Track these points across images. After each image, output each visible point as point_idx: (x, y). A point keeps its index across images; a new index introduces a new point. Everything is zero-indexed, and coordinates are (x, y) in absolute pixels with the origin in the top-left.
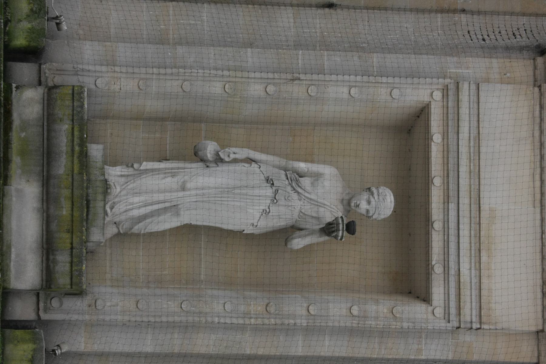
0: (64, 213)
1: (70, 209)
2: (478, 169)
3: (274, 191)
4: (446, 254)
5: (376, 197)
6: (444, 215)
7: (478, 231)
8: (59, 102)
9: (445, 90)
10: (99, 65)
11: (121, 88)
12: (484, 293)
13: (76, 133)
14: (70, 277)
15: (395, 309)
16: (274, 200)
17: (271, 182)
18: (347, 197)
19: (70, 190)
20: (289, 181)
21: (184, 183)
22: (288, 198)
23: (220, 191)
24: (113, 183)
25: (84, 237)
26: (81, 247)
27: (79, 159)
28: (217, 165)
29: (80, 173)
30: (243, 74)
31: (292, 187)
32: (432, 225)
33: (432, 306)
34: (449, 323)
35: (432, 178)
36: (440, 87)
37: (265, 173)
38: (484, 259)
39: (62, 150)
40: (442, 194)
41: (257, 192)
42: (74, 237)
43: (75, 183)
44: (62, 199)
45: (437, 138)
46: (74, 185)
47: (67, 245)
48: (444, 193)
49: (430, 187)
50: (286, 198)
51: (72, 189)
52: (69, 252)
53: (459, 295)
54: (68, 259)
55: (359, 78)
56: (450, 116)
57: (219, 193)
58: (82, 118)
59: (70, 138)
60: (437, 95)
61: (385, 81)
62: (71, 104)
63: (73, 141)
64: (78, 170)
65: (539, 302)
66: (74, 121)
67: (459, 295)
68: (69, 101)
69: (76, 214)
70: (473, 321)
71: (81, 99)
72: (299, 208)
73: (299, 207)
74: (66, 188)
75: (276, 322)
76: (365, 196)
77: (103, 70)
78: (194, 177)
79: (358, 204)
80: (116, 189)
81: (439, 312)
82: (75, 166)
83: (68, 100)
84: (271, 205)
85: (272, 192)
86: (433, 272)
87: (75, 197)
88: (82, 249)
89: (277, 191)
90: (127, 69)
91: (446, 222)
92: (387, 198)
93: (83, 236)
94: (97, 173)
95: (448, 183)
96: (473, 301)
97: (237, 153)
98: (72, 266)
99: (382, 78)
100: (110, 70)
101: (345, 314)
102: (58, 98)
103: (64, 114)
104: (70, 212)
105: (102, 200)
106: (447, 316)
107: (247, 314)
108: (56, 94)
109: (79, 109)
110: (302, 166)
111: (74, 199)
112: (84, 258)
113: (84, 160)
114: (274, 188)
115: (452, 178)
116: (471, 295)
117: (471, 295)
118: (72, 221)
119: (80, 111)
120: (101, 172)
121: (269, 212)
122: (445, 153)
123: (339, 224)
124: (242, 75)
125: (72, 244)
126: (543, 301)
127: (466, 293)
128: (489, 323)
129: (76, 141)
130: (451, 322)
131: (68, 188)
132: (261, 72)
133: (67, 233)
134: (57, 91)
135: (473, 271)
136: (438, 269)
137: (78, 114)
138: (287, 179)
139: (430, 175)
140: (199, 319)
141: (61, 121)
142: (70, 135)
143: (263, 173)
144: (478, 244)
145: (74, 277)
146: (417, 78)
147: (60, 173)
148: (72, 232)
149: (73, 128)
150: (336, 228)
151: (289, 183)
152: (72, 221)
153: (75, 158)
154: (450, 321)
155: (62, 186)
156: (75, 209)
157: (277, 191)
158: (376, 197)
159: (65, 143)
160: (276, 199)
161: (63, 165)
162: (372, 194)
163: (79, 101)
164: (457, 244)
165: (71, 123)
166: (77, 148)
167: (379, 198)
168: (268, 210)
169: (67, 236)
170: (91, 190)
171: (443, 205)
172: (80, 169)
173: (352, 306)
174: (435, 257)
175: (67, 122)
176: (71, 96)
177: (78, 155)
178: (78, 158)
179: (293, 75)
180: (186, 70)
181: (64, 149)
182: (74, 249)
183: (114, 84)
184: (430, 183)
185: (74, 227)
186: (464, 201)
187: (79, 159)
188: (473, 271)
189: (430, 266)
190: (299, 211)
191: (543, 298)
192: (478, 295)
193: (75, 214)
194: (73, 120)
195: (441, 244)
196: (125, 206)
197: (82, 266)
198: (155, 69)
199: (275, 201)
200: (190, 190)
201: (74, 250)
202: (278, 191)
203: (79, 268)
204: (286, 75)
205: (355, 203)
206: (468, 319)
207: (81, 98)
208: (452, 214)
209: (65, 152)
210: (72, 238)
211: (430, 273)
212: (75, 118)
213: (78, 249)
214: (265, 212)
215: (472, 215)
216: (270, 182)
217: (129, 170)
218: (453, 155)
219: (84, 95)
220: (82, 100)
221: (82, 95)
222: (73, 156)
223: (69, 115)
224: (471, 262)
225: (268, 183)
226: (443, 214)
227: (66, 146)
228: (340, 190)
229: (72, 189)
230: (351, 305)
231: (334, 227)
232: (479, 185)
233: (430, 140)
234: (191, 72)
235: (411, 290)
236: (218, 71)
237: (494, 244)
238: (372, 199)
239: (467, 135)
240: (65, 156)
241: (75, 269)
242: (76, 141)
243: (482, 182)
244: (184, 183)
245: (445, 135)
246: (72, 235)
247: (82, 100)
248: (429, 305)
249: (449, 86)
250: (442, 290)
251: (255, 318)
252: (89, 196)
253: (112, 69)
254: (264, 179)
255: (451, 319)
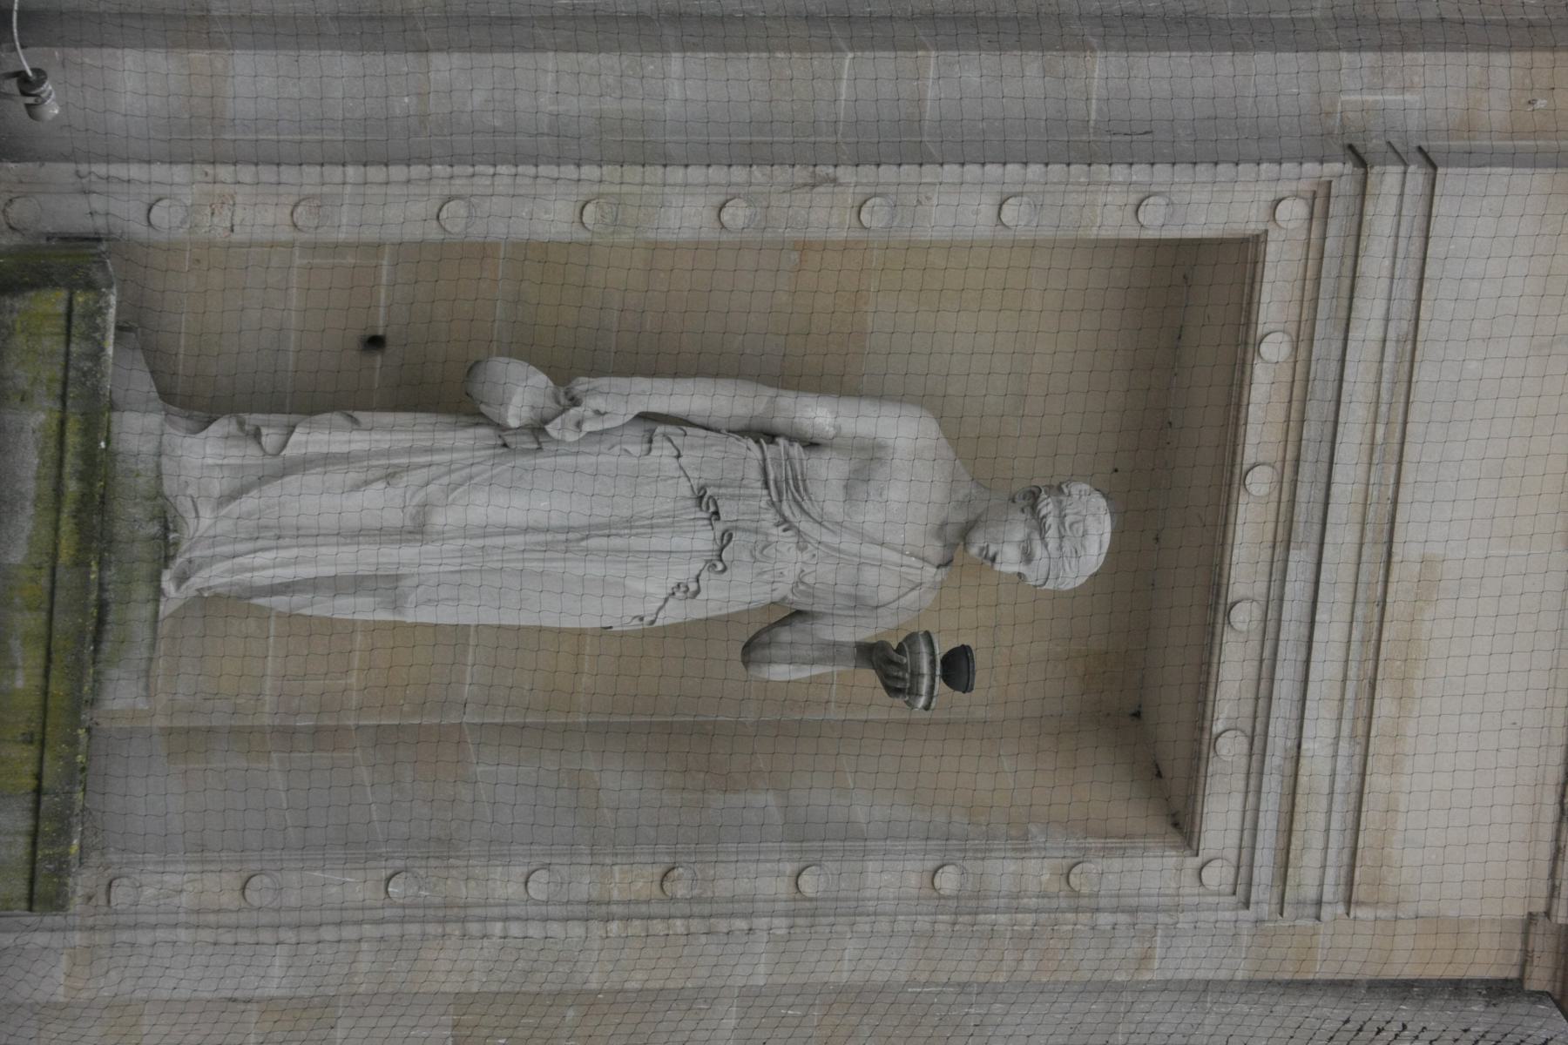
0: (20, 683)
1: (40, 671)
2: (1398, 435)
3: (718, 534)
4: (1263, 696)
5: (1053, 543)
6: (1270, 581)
7: (1376, 624)
8: (20, 340)
9: (1320, 200)
10: (163, 162)
11: (232, 226)
12: (1370, 818)
13: (73, 440)
14: (26, 876)
15: (1076, 870)
16: (717, 561)
17: (712, 509)
18: (961, 517)
19: (44, 615)
20: (770, 495)
21: (425, 507)
22: (761, 552)
23: (538, 543)
24: (189, 499)
25: (80, 758)
26: (67, 788)
27: (76, 521)
28: (535, 446)
29: (80, 563)
30: (647, 174)
31: (780, 513)
32: (1227, 614)
33: (1197, 855)
34: (1248, 908)
35: (1245, 467)
36: (1305, 186)
37: (693, 474)
38: (1385, 707)
39: (23, 490)
40: (1271, 517)
41: (659, 542)
42: (48, 757)
43: (60, 596)
44: (15, 644)
45: (1274, 350)
46: (56, 600)
47: (23, 780)
48: (1278, 514)
49: (1235, 495)
50: (757, 554)
51: (51, 612)
52: (28, 803)
53: (1288, 829)
54: (25, 824)
55: (1035, 170)
56: (1327, 284)
57: (538, 548)
58: (95, 393)
59: (52, 451)
60: (1293, 212)
61: (1120, 179)
62: (62, 349)
63: (60, 463)
64: (72, 552)
65: (1547, 832)
66: (69, 403)
67: (1288, 829)
68: (56, 338)
69: (58, 688)
70: (1325, 899)
71: (94, 332)
72: (798, 571)
73: (799, 566)
74: (29, 608)
75: (688, 928)
76: (1018, 531)
77: (177, 179)
78: (461, 489)
79: (991, 553)
80: (198, 517)
81: (1219, 876)
82: (63, 541)
83: (52, 334)
84: (704, 575)
85: (712, 538)
86: (1211, 754)
87: (57, 636)
88: (71, 793)
89: (727, 537)
90: (257, 173)
91: (1273, 604)
92: (1087, 544)
93: (77, 754)
94: (138, 512)
95: (1292, 521)
96: (1334, 808)
97: (605, 413)
98: (34, 844)
99: (1114, 167)
100: (199, 177)
101: (915, 892)
102: (18, 326)
103: (35, 379)
104: (38, 681)
105: (148, 601)
106: (1241, 889)
107: (599, 904)
108: (11, 312)
109: (87, 365)
110: (818, 415)
111: (53, 644)
112: (74, 820)
113: (96, 519)
114: (720, 527)
115: (1304, 506)
116: (1327, 830)
117: (1327, 830)
118: (45, 709)
119: (90, 369)
120: (150, 509)
121: (698, 592)
122: (1262, 703)
123: (921, 675)
124: (643, 178)
125: (39, 777)
126: (1559, 831)
127: (1311, 817)
128: (1376, 904)
129: (72, 462)
130: (1252, 907)
131: (38, 608)
132: (709, 165)
133: (24, 746)
134: (17, 305)
135: (1344, 746)
136: (1230, 750)
137: (83, 379)
138: (766, 485)
139: (1238, 460)
140: (440, 930)
141: (22, 400)
142: (52, 443)
143: (687, 476)
144: (1370, 665)
145: (40, 880)
146: (1231, 165)
147: (12, 560)
148: (43, 743)
149: (62, 423)
150: (908, 685)
151: (771, 500)
152: (45, 709)
153: (64, 516)
154: (1251, 905)
155: (17, 600)
156: (54, 673)
157: (727, 537)
158: (1053, 543)
159: (35, 469)
160: (721, 560)
161: (24, 536)
162: (1042, 529)
163: (87, 337)
164: (1300, 667)
165: (58, 406)
166: (72, 486)
167: (1060, 548)
168: (693, 587)
169: (25, 755)
170: (113, 570)
171: (1269, 552)
172: (78, 550)
173: (942, 866)
174: (1226, 711)
175: (46, 404)
176: (62, 322)
177: (74, 507)
178: (75, 517)
179: (814, 172)
180: (455, 168)
181: (30, 487)
182: (46, 794)
183: (213, 214)
184: (1236, 485)
185: (49, 729)
186: (1342, 537)
187: (76, 521)
188: (1344, 746)
189: (1207, 736)
190: (796, 579)
191: (1560, 821)
192: (1342, 880)
193: (53, 688)
194: (63, 398)
195: (1250, 669)
196: (227, 571)
197: (69, 844)
198: (350, 170)
199: (720, 567)
200: (442, 536)
201: (45, 799)
202: (731, 536)
203: (61, 849)
204: (790, 170)
205: (982, 549)
206: (1311, 893)
207: (97, 329)
208: (1297, 589)
209: (32, 495)
210: (41, 760)
211: (1204, 755)
212: (73, 391)
213: (57, 795)
214: (683, 589)
215: (1363, 578)
216: (708, 508)
217: (249, 452)
218: (1318, 411)
219: (104, 321)
220: (97, 335)
221: (99, 320)
222: (58, 511)
223: (51, 380)
224: (1340, 719)
225: (701, 510)
226: (1266, 578)
227: (38, 478)
228: (938, 495)
229: (51, 612)
230: (938, 863)
231: (903, 679)
232: (1398, 483)
233: (1250, 349)
234: (473, 175)
235: (1140, 706)
236: (563, 168)
237: (1418, 701)
238: (1038, 551)
239: (1375, 332)
240: (30, 511)
241: (45, 856)
242: (72, 462)
243: (1408, 475)
244: (425, 507)
245: (1303, 338)
246: (42, 753)
247: (97, 335)
248: (1188, 852)
249: (1333, 184)
250: (1236, 801)
251: (621, 919)
252: (107, 590)
253: (206, 174)
254: (688, 493)
255: (1253, 898)
